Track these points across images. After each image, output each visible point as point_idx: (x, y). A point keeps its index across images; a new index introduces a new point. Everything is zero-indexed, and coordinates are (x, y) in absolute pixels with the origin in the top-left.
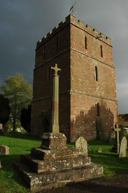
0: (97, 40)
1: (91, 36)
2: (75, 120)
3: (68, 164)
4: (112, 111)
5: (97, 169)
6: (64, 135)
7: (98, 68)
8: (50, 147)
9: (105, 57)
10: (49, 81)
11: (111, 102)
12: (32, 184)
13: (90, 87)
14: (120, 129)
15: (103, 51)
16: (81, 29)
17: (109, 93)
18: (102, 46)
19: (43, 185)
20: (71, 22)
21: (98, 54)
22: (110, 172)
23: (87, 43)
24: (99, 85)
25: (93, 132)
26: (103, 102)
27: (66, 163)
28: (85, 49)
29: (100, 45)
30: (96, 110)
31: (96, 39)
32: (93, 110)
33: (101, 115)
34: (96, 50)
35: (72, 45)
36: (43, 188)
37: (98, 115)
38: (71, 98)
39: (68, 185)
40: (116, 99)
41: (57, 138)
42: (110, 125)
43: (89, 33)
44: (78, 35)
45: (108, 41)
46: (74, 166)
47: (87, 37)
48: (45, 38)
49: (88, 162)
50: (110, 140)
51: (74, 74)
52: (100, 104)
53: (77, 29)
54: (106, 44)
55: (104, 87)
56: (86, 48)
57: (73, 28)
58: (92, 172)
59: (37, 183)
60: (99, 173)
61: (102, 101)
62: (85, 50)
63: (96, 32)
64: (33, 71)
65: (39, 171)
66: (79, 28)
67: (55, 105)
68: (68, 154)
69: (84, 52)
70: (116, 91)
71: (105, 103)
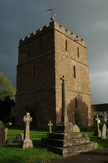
0: (75, 42)
1: (70, 39)
2: (59, 111)
3: (78, 141)
4: (86, 103)
5: (94, 145)
6: (71, 124)
7: (76, 67)
8: (65, 132)
9: (80, 57)
10: (34, 77)
11: (86, 95)
12: (63, 153)
13: (70, 84)
14: (52, 124)
15: (80, 52)
16: (62, 33)
17: (84, 89)
18: (79, 47)
19: (69, 153)
20: (55, 28)
21: (76, 55)
22: (100, 147)
23: (67, 45)
24: (76, 82)
25: (73, 121)
26: (80, 96)
27: (77, 141)
28: (65, 51)
29: (77, 47)
30: (75, 103)
31: (74, 42)
32: (73, 103)
33: (79, 107)
34: (74, 51)
35: (56, 48)
36: (68, 155)
37: (76, 107)
38: (56, 93)
39: (81, 153)
40: (89, 93)
41: (68, 125)
42: (86, 115)
43: (68, 37)
44: (60, 39)
45: (83, 43)
46: (81, 142)
47: (67, 41)
48: (28, 37)
49: (88, 140)
50: (88, 128)
51: (58, 73)
52: (78, 98)
53: (60, 33)
54: (82, 45)
55: (81, 83)
56: (66, 50)
57: (56, 33)
58: (92, 146)
59: (66, 152)
60: (95, 147)
61: (79, 95)
62: (65, 52)
63: (74, 35)
64: (62, 85)
65: (64, 146)
66: (61, 33)
67: (65, 104)
68: (76, 135)
69: (65, 54)
70: (90, 87)
71: (81, 97)
